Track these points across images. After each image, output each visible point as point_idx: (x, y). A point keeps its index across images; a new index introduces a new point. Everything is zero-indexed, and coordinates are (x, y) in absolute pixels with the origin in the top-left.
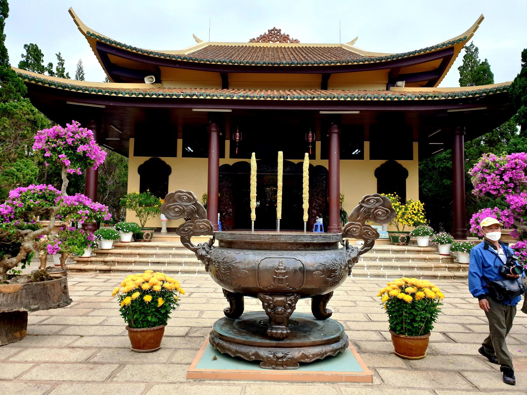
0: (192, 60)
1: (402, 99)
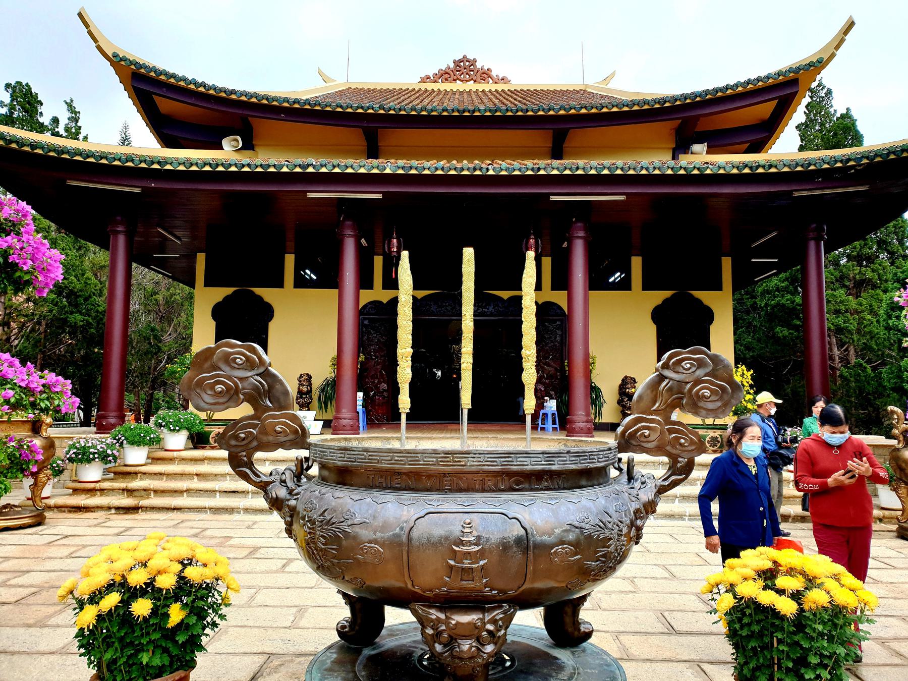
0: (309, 104)
1: (708, 172)
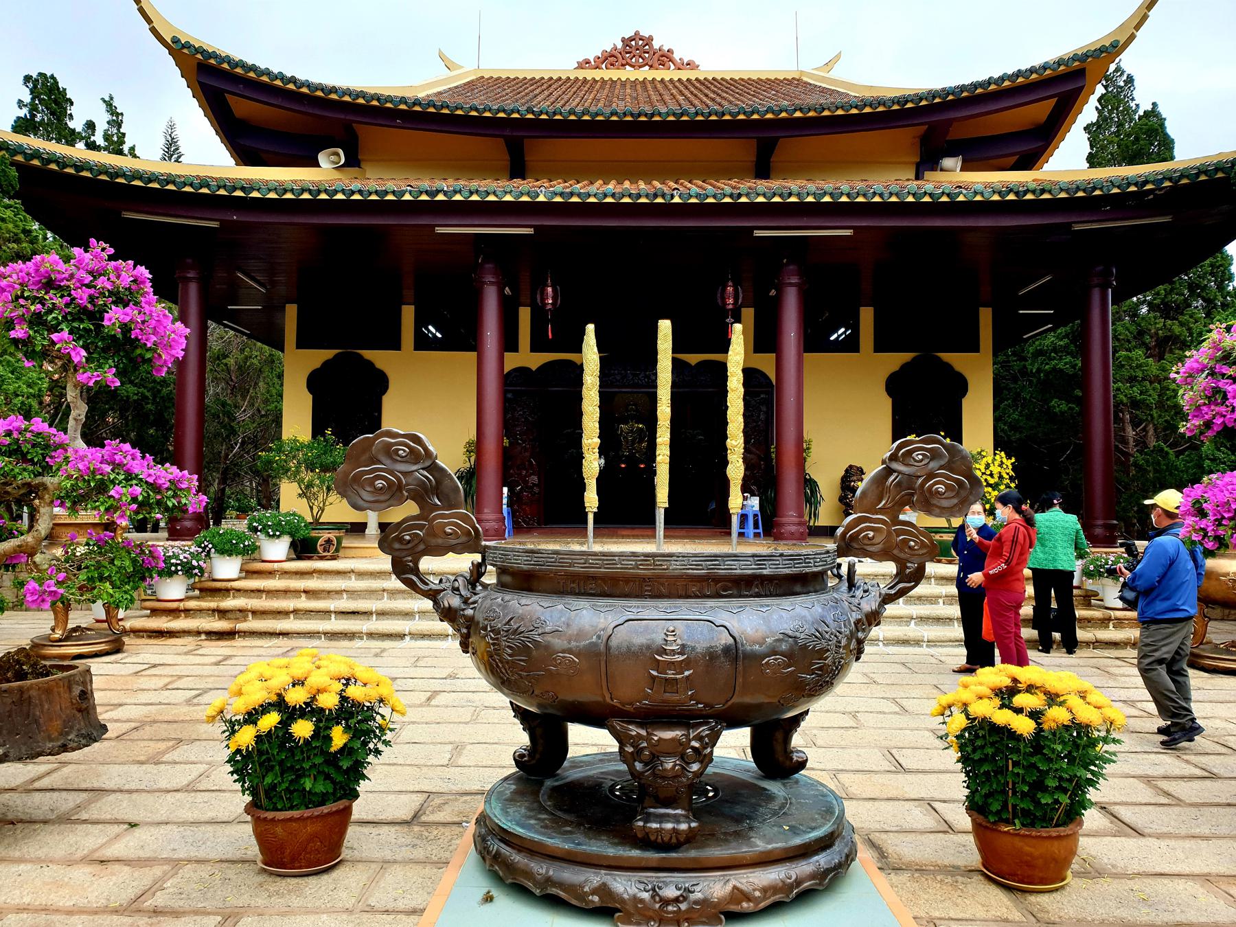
0: (434, 106)
1: (961, 198)
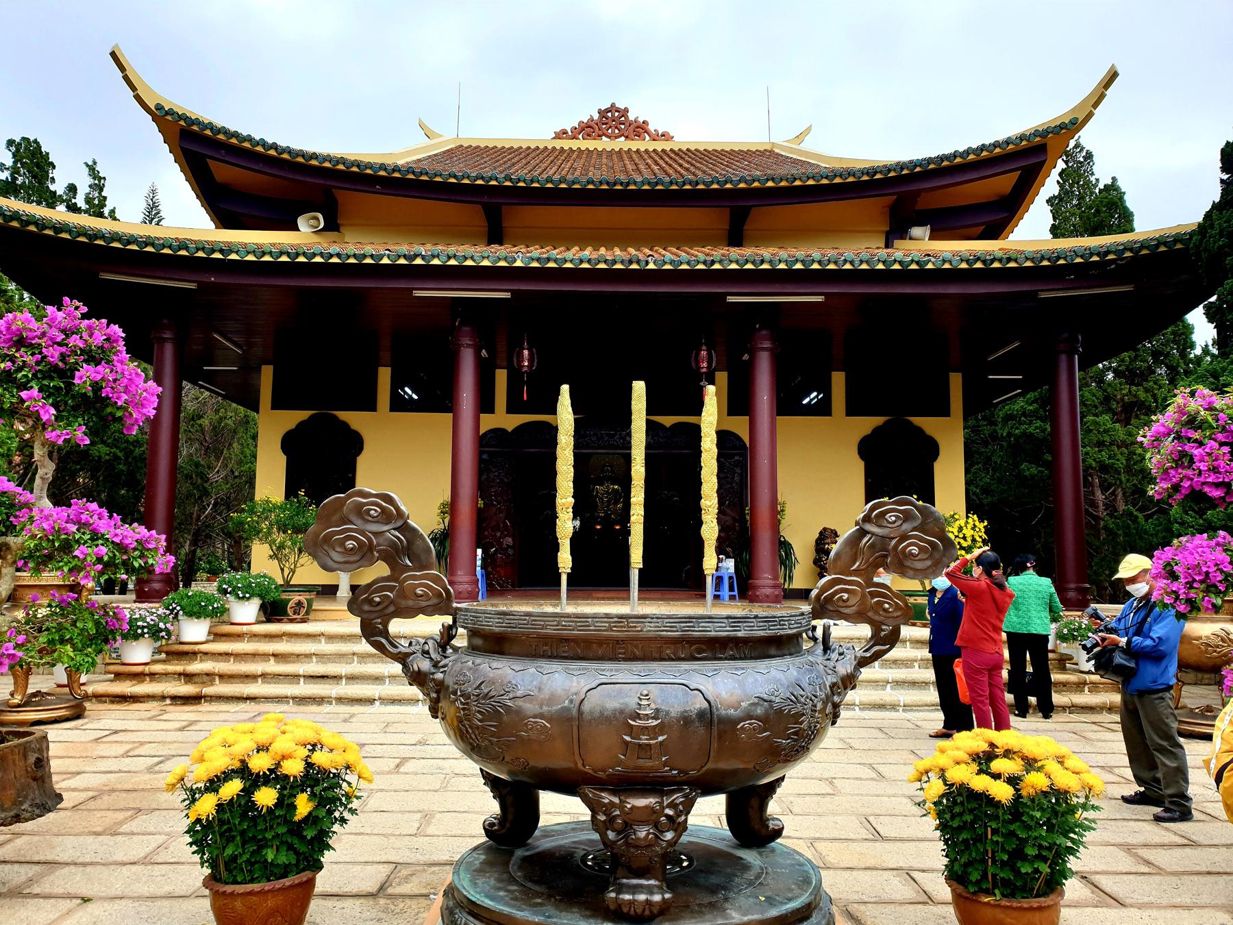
0: (413, 173)
1: (930, 266)
